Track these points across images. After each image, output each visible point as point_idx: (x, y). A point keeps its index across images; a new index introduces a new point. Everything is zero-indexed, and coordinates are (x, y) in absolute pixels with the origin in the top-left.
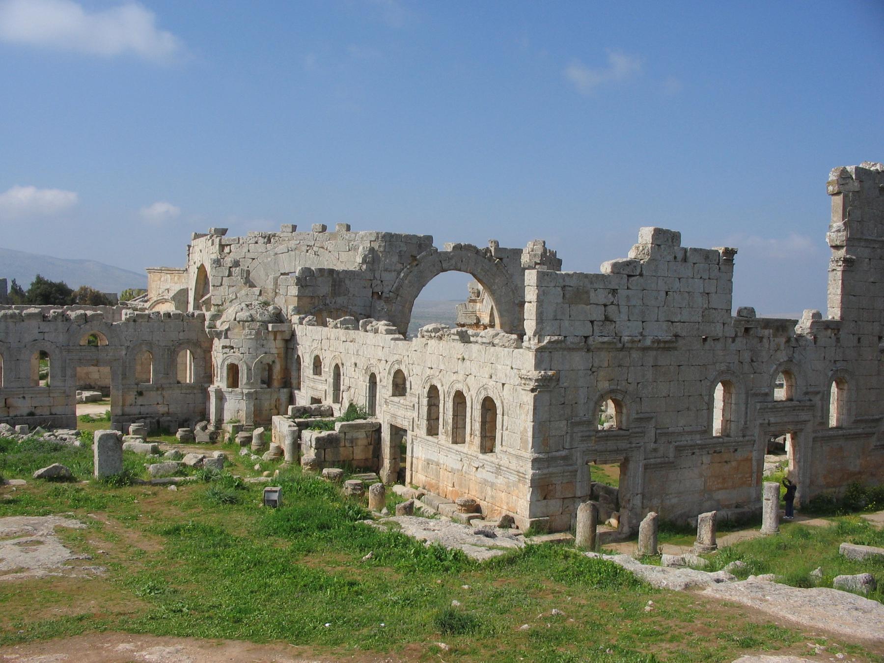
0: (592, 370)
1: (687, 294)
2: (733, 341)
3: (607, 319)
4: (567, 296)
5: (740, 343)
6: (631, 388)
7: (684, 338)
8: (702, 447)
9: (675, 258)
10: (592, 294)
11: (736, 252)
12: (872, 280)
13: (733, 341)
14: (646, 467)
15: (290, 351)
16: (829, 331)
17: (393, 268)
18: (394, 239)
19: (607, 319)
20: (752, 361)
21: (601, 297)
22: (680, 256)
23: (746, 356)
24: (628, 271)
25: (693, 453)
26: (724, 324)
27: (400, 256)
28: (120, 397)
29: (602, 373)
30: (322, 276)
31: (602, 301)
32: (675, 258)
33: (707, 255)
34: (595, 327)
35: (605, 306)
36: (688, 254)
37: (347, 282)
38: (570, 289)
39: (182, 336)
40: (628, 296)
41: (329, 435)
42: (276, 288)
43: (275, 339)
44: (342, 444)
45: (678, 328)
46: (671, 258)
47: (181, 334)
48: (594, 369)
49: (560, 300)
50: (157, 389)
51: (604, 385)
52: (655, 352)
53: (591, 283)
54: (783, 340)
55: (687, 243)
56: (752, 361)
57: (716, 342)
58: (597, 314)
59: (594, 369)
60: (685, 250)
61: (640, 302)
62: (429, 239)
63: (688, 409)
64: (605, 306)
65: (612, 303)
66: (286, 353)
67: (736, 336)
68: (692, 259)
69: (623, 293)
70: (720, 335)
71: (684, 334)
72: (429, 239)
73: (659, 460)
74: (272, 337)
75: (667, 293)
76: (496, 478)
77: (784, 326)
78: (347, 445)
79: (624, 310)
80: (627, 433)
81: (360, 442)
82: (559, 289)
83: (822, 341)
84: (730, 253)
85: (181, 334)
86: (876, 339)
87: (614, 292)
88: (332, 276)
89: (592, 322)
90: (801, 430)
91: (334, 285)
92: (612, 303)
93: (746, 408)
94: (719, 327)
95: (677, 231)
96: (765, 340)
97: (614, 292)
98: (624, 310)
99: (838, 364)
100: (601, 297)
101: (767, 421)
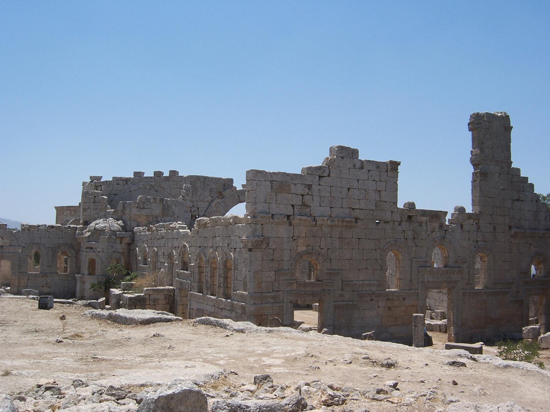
0: (294, 239)
1: (363, 191)
2: (400, 225)
3: (304, 204)
4: (274, 187)
5: (405, 225)
6: (323, 252)
7: (362, 220)
8: (378, 296)
9: (354, 166)
10: (292, 187)
11: (398, 164)
12: (502, 187)
13: (400, 225)
14: (336, 307)
15: (131, 251)
16: (472, 220)
17: (206, 199)
18: (207, 180)
19: (304, 204)
20: (414, 238)
21: (300, 189)
22: (358, 165)
23: (410, 234)
24: (319, 173)
25: (372, 300)
26: (392, 212)
27: (211, 192)
28: (17, 281)
29: (301, 241)
30: (155, 202)
31: (300, 192)
32: (354, 166)
33: (378, 165)
34: (295, 210)
35: (303, 195)
36: (364, 164)
37: (173, 206)
38: (276, 182)
39: (61, 241)
40: (319, 190)
41: (138, 296)
42: (124, 209)
43: (121, 243)
44: (148, 303)
45: (357, 213)
46: (352, 166)
47: (61, 240)
48: (294, 238)
49: (269, 189)
50: (43, 276)
51: (302, 248)
52: (340, 229)
53: (292, 179)
54: (437, 225)
55: (362, 157)
56: (414, 238)
57: (386, 224)
58: (297, 201)
59: (294, 238)
60: (362, 162)
61: (328, 195)
62: (231, 181)
63: (367, 269)
64: (303, 195)
65: (308, 194)
66: (129, 253)
67: (401, 221)
68: (366, 167)
69: (315, 187)
70: (389, 219)
71: (362, 217)
72: (231, 181)
73: (345, 303)
74: (118, 241)
75: (349, 189)
76: (231, 313)
77: (438, 216)
78: (151, 303)
79: (316, 199)
80: (321, 282)
81: (160, 302)
82: (269, 183)
83: (466, 227)
84: (394, 166)
85: (61, 240)
86: (507, 227)
87: (309, 187)
88: (163, 202)
89: (293, 206)
90: (454, 287)
91: (163, 209)
92: (308, 194)
93: (411, 271)
94: (388, 214)
95: (355, 148)
96: (424, 225)
97: (309, 187)
98: (316, 199)
99: (479, 243)
100: (300, 189)
101: (426, 280)
